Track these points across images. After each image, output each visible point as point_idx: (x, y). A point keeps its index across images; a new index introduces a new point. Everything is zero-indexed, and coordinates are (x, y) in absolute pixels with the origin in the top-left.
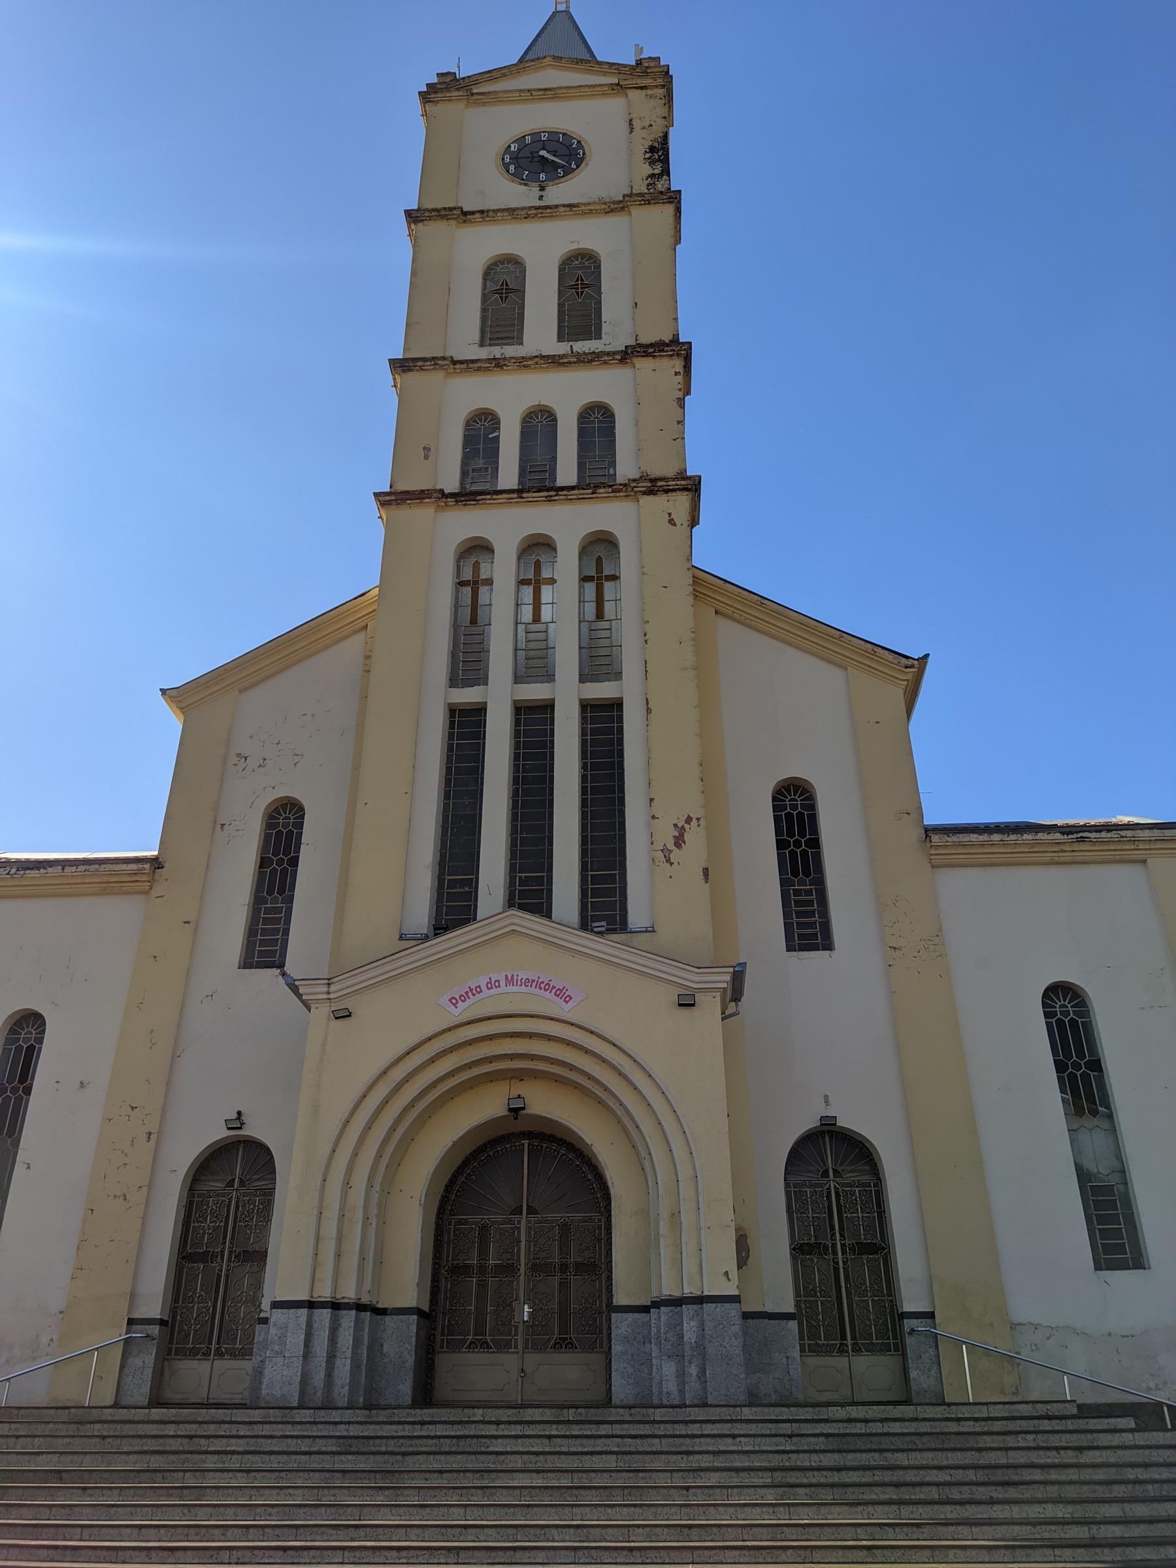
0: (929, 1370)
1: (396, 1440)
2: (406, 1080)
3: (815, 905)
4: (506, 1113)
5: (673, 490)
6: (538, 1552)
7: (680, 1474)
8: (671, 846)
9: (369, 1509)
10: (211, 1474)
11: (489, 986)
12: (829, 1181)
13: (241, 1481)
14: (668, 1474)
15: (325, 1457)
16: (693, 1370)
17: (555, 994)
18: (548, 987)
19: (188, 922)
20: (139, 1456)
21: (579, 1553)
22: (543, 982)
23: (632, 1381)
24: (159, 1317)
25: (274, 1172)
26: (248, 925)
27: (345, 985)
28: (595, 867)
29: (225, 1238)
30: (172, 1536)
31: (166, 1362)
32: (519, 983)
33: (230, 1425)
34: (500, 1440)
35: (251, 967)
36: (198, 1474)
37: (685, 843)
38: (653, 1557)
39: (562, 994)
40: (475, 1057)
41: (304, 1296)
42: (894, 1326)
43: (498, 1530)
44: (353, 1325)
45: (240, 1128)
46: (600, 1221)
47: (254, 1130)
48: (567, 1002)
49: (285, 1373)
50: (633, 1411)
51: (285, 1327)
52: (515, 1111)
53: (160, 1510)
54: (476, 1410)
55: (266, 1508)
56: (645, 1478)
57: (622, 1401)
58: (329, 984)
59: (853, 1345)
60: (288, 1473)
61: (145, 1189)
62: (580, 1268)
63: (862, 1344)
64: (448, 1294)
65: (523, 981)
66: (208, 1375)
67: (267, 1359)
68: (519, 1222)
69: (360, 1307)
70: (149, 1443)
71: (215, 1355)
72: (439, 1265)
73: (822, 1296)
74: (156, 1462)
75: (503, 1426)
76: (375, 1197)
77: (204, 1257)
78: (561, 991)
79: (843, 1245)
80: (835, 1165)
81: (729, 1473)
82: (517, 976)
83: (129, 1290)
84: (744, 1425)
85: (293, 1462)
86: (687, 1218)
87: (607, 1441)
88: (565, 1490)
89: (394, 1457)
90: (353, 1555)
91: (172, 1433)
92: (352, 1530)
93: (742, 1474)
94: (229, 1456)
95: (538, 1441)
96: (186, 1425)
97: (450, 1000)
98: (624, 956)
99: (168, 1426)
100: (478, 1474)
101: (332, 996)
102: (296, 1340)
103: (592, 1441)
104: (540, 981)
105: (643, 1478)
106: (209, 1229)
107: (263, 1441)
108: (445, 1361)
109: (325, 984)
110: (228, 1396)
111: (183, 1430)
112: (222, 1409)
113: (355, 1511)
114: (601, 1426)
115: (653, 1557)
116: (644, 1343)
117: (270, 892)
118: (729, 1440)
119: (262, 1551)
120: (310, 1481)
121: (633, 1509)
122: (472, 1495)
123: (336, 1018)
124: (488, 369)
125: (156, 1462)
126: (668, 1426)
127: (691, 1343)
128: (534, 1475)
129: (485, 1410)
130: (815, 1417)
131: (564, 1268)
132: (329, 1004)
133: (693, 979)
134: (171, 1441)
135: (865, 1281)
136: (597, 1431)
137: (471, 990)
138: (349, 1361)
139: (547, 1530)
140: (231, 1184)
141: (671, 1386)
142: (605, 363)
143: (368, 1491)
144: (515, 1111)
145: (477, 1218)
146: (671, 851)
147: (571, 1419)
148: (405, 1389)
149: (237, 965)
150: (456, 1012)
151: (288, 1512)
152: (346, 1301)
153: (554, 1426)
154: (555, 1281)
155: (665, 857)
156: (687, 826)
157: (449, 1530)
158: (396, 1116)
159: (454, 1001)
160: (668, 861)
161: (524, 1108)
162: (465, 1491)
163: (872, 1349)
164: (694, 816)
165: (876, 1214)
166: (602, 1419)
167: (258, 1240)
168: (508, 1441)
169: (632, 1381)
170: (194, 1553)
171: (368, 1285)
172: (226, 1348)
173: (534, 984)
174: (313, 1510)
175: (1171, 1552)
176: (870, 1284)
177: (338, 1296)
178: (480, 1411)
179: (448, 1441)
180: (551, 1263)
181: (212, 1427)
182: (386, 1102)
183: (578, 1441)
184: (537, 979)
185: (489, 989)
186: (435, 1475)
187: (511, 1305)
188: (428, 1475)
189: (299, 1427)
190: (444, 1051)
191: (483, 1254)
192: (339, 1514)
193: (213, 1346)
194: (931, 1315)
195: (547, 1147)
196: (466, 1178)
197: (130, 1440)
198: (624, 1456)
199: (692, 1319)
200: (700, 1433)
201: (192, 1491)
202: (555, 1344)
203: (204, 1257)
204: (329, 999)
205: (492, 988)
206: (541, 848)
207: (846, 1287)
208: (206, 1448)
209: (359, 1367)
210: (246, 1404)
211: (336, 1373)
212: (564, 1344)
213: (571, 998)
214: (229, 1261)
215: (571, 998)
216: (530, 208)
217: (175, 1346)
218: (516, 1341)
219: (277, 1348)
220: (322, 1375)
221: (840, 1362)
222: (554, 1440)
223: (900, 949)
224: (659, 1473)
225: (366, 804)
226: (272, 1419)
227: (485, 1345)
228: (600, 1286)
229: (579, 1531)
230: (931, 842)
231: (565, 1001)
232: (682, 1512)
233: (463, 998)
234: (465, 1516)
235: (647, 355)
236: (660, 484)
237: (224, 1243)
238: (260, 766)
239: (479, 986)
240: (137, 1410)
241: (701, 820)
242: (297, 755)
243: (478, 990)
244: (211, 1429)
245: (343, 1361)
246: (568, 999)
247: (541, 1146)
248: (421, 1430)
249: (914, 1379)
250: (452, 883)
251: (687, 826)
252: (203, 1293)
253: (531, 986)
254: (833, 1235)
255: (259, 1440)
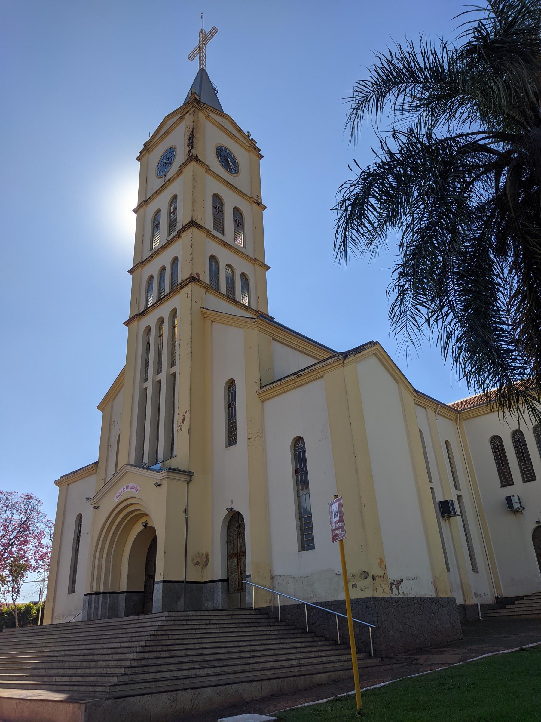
5: (187, 284)
8: (182, 424)
98: (102, 493)
124: (150, 260)
142: (175, 240)
175: (540, 616)
216: (160, 188)
235: (183, 231)
236: (183, 284)
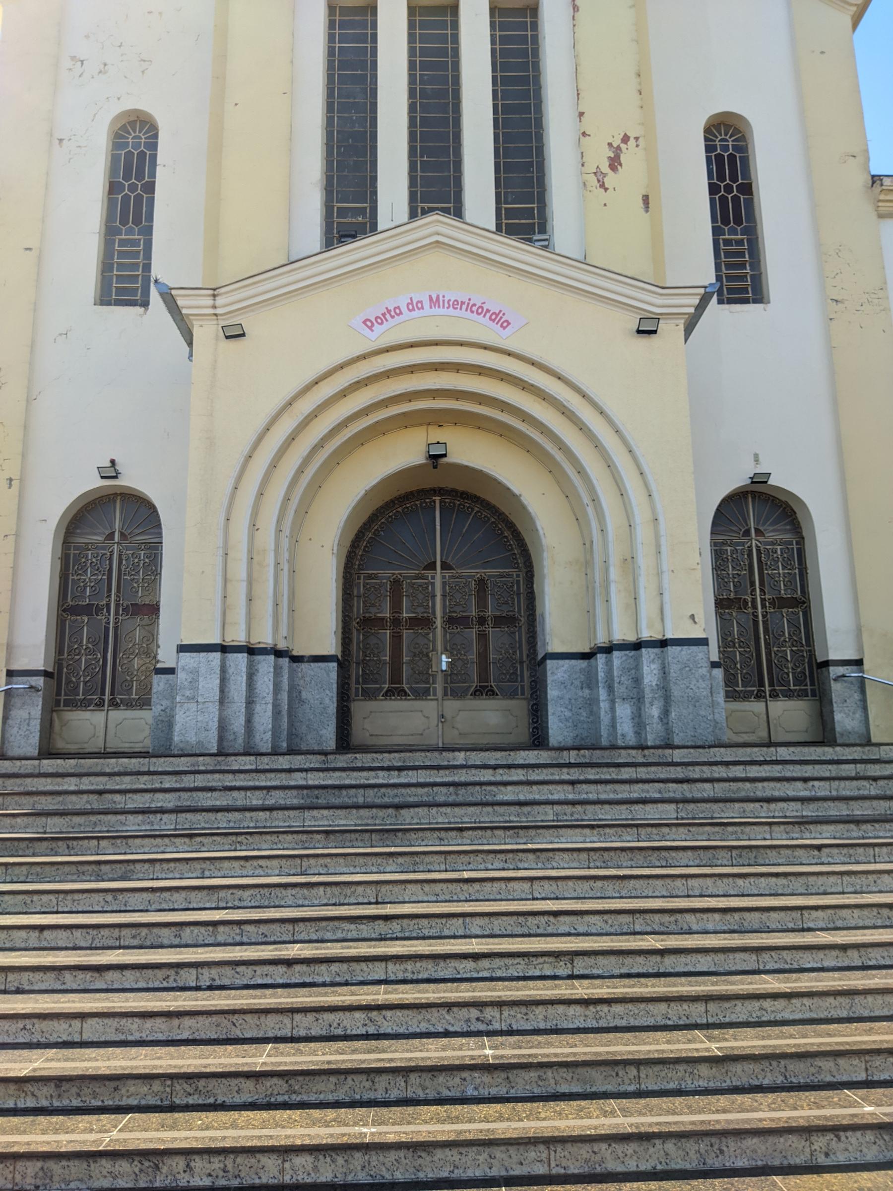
0: (854, 713)
1: (376, 790)
2: (314, 415)
3: (747, 256)
4: (423, 461)
6: (699, 956)
7: (782, 827)
8: (605, 168)
9: (389, 887)
10: (138, 841)
11: (411, 307)
12: (751, 540)
13: (181, 850)
14: (767, 828)
15: (292, 813)
16: (655, 711)
17: (490, 318)
18: (481, 310)
19: (30, 249)
20: (31, 819)
21: (764, 955)
22: (474, 305)
23: (569, 724)
24: (42, 668)
25: (159, 526)
26: (101, 259)
27: (232, 299)
28: (510, 200)
29: (110, 590)
30: (93, 939)
31: (55, 714)
32: (446, 305)
33: (151, 777)
34: (509, 788)
35: (109, 304)
36: (119, 841)
37: (621, 165)
38: (879, 958)
39: (497, 318)
40: (394, 391)
41: (216, 640)
42: (811, 673)
43: (606, 917)
44: (272, 670)
45: (115, 477)
46: (518, 576)
47: (130, 480)
48: (504, 328)
49: (200, 718)
50: (646, 752)
51: (195, 672)
52: (435, 459)
53: (69, 897)
54: (457, 753)
55: (235, 891)
56: (736, 832)
57: (560, 743)
58: (214, 296)
59: (771, 691)
60: (248, 837)
61: (12, 539)
62: (499, 621)
63: (780, 690)
64: (361, 646)
65: (451, 303)
66: (103, 725)
67: (178, 705)
68: (433, 578)
69: (278, 653)
70: (44, 802)
71: (109, 706)
72: (351, 618)
73: (740, 647)
74: (55, 825)
75: (501, 771)
76: (285, 543)
77: (88, 610)
78: (497, 315)
79: (763, 600)
80: (758, 525)
81: (847, 826)
82: (444, 297)
83: (5, 641)
84: (798, 767)
85: (248, 821)
86: (645, 561)
87: (646, 786)
88: (650, 852)
89: (384, 811)
90: (402, 967)
91: (72, 788)
92: (381, 922)
93: (864, 827)
94: (159, 816)
95: (559, 788)
96: (91, 778)
97: (364, 322)
99: (67, 779)
100: (511, 832)
101: (218, 311)
102: (210, 685)
103: (626, 787)
104: (471, 303)
105: (732, 833)
106: (91, 582)
107: (200, 794)
108: (360, 709)
109: (209, 295)
110: (127, 745)
111: (86, 784)
112: (136, 757)
113: (368, 891)
114: (623, 769)
115: (879, 958)
116: (582, 688)
117: (124, 221)
118: (799, 784)
119: (251, 967)
120: (280, 846)
121: (774, 879)
122: (521, 861)
123: (227, 337)
125: (55, 825)
126: (705, 768)
127: (651, 686)
128: (587, 831)
129: (468, 753)
130: (864, 757)
131: (482, 621)
132: (215, 322)
133: (654, 303)
134: (74, 798)
135: (784, 633)
136: (617, 775)
137: (389, 311)
138: (270, 707)
139: (678, 916)
140: (111, 536)
141: (626, 728)
143: (373, 859)
144: (435, 459)
145: (388, 573)
146: (605, 175)
147: (572, 761)
148: (328, 735)
149: (93, 301)
150: (373, 336)
151: (267, 895)
152: (262, 646)
153: (565, 770)
154: (473, 633)
155: (599, 181)
156: (623, 146)
157: (530, 918)
158: (305, 454)
159: (368, 324)
160: (602, 186)
161: (445, 455)
162: (511, 855)
163: (789, 695)
164: (632, 135)
165: (797, 571)
166: (609, 761)
167: (147, 593)
168: (520, 788)
169: (569, 724)
170: (137, 973)
171: (284, 631)
172: (121, 699)
173: (464, 307)
174: (305, 891)
176: (789, 635)
177: (252, 641)
178: (462, 755)
179: (444, 790)
180: (468, 617)
181: (127, 779)
182: (292, 438)
183: (609, 787)
184: (467, 301)
185: (410, 310)
186: (453, 834)
187: (427, 656)
188: (443, 834)
189: (242, 776)
190: (358, 382)
191: (396, 606)
192: (346, 896)
193: (107, 697)
194: (859, 663)
195: (460, 505)
196: (374, 534)
197: (17, 798)
198: (686, 805)
199: (653, 661)
200: (744, 775)
201: (114, 866)
202: (475, 692)
203: (88, 610)
204: (216, 315)
205: (413, 309)
206: (446, 174)
207: (765, 640)
208: (122, 806)
209: (279, 713)
210: (148, 752)
211: (256, 719)
212: (484, 691)
213: (509, 324)
214: (117, 613)
215: (509, 324)
217: (63, 698)
218: (435, 689)
219: (188, 693)
220: (242, 720)
221: (758, 707)
222: (579, 786)
223: (842, 302)
224: (755, 827)
225: (236, 104)
226: (202, 768)
227: (402, 693)
228: (520, 638)
229: (728, 917)
230: (882, 185)
231: (502, 326)
232: (845, 883)
233: (379, 321)
234: (532, 893)
237: (109, 596)
238: (100, 72)
239: (398, 308)
240: (23, 762)
241: (640, 139)
242: (144, 61)
243: (398, 311)
244: (126, 783)
245: (264, 706)
246: (505, 324)
247: (454, 504)
248: (399, 776)
249: (838, 722)
250: (342, 212)
251: (623, 146)
252: (90, 646)
253: (461, 309)
254: (754, 590)
255: (194, 794)
